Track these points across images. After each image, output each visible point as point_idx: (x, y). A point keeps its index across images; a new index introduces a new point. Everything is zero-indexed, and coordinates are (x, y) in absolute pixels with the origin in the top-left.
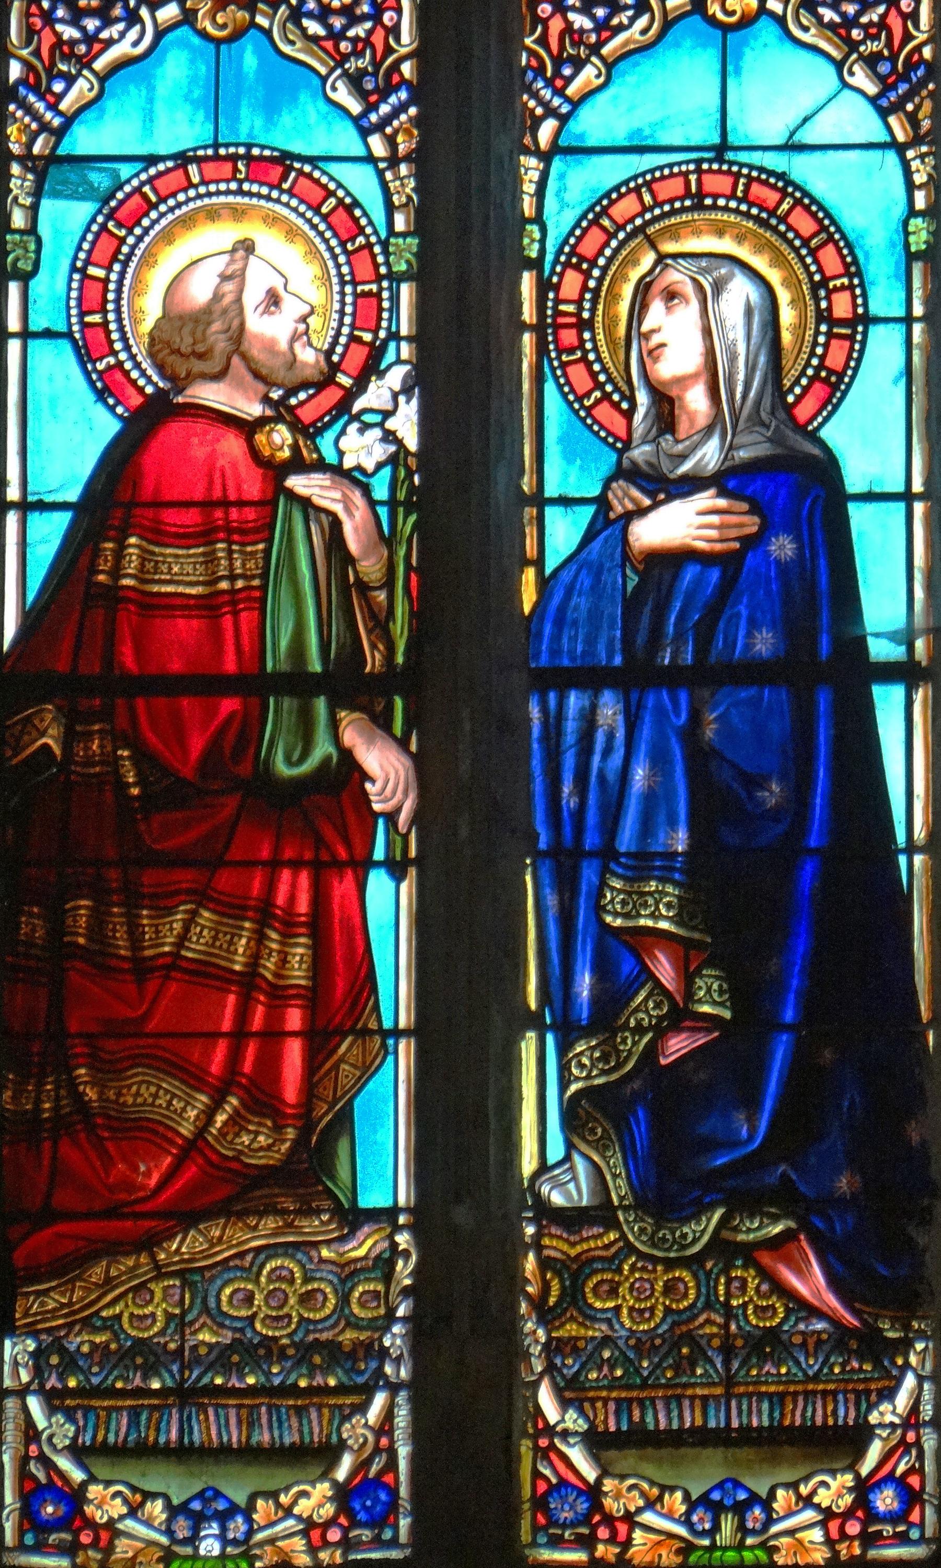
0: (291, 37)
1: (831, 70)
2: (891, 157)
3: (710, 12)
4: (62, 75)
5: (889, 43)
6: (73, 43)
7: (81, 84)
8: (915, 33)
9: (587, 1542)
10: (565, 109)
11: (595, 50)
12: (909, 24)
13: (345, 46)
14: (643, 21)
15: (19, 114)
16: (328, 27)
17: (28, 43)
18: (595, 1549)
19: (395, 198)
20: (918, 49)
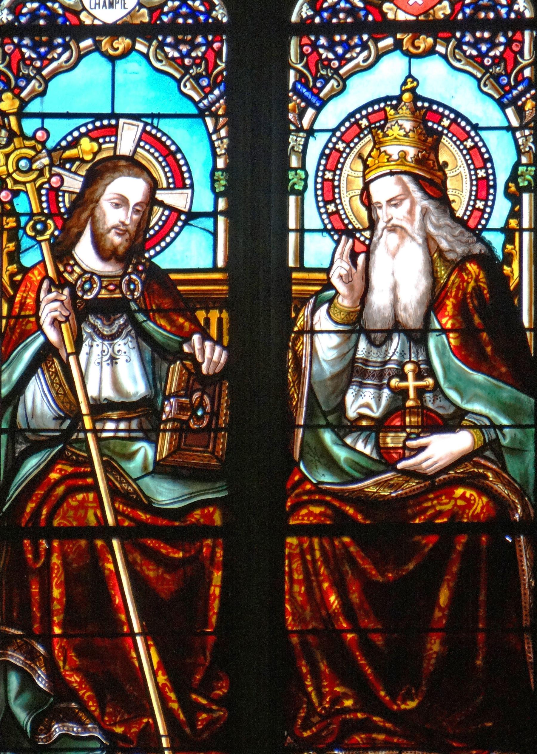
0: (160, 58)
1: (174, 84)
2: (508, 135)
3: (103, 50)
7: (333, 83)
8: (520, 59)
11: (39, 70)
12: (518, 56)
14: (365, 53)
17: (301, 61)
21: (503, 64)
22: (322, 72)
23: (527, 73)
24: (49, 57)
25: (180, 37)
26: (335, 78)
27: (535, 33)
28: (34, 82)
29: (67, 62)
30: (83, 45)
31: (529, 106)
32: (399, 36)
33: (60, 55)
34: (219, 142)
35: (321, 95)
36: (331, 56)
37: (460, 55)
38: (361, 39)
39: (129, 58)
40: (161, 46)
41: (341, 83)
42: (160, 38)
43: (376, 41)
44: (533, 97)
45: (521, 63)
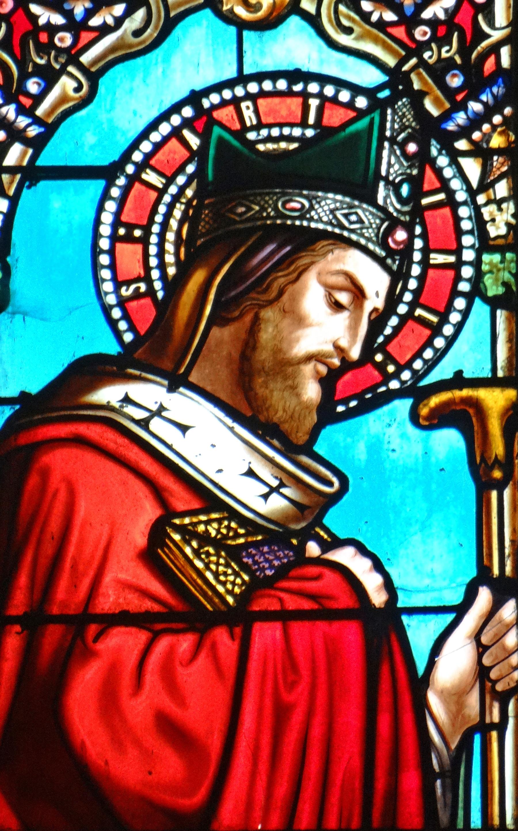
0: (345, 22)
7: (66, 85)
8: (486, 29)
10: (33, 131)
11: (72, 56)
13: (422, 33)
22: (39, 61)
24: (95, 21)
26: (71, 75)
28: (64, 80)
29: (137, 33)
33: (119, 21)
35: (39, 112)
36: (58, 19)
37: (349, 18)
39: (282, 28)
45: (488, 36)
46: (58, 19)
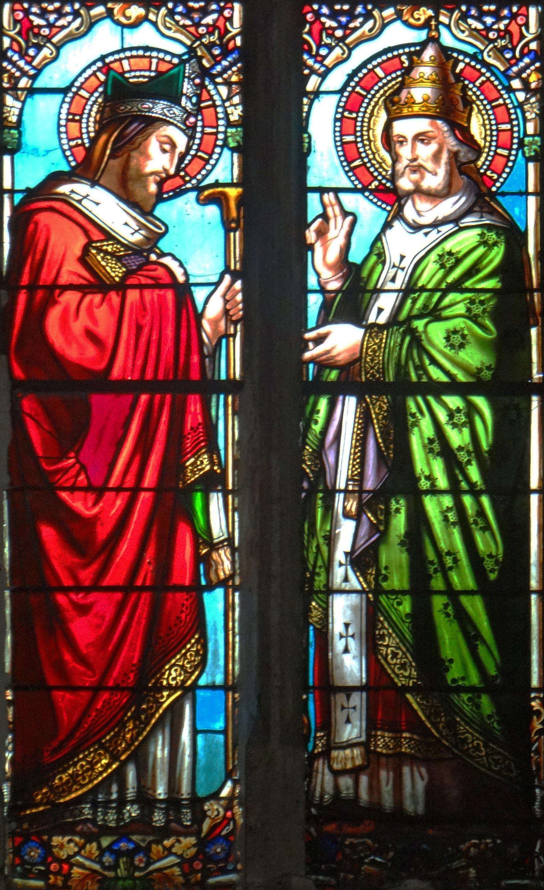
4: (327, 46)
5: (511, 41)
6: (40, 27)
7: (337, 52)
9: (43, 876)
10: (32, 72)
11: (48, 39)
14: (370, 23)
15: (9, 67)
16: (339, 22)
18: (50, 879)
19: (527, 114)
20: (527, 44)
21: (507, 36)
23: (533, 46)
25: (338, 7)
27: (540, 9)
29: (78, 29)
30: (94, 12)
31: (533, 78)
32: (110, 5)
34: (233, 108)
36: (334, 24)
38: (510, 11)
40: (171, 13)
41: (347, 52)
42: (464, 8)
43: (381, 11)
44: (537, 70)
45: (230, 32)
46: (334, 24)
